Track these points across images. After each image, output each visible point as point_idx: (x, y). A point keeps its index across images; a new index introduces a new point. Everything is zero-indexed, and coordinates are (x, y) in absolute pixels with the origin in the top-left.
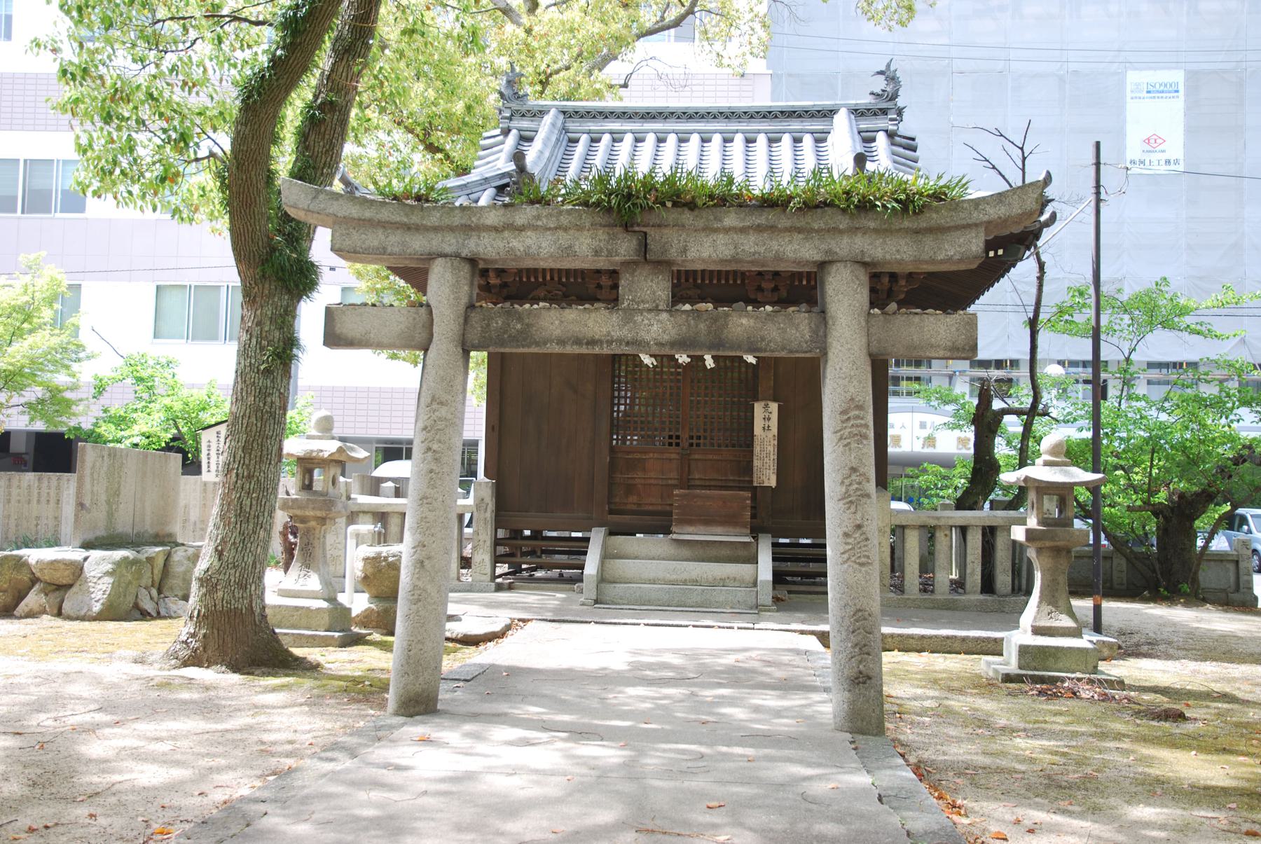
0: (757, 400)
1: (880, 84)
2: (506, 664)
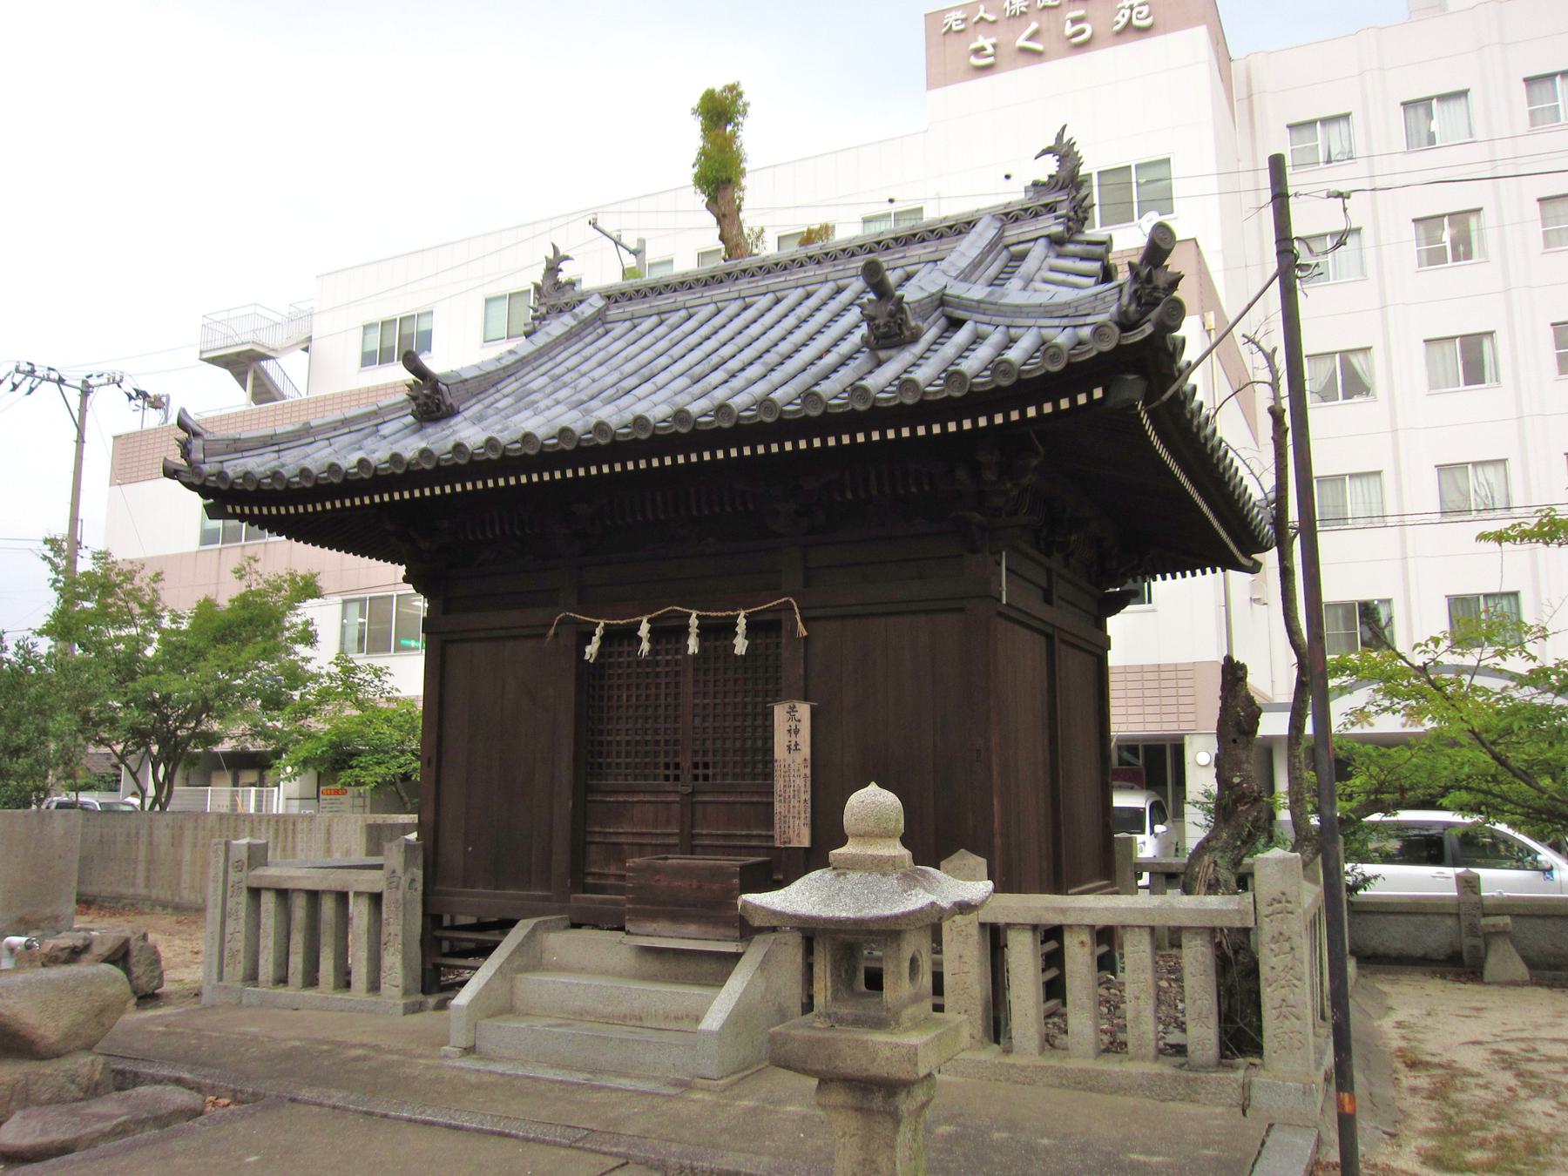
0: (778, 697)
1: (1050, 166)
2: (1213, 977)
